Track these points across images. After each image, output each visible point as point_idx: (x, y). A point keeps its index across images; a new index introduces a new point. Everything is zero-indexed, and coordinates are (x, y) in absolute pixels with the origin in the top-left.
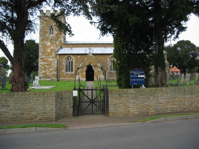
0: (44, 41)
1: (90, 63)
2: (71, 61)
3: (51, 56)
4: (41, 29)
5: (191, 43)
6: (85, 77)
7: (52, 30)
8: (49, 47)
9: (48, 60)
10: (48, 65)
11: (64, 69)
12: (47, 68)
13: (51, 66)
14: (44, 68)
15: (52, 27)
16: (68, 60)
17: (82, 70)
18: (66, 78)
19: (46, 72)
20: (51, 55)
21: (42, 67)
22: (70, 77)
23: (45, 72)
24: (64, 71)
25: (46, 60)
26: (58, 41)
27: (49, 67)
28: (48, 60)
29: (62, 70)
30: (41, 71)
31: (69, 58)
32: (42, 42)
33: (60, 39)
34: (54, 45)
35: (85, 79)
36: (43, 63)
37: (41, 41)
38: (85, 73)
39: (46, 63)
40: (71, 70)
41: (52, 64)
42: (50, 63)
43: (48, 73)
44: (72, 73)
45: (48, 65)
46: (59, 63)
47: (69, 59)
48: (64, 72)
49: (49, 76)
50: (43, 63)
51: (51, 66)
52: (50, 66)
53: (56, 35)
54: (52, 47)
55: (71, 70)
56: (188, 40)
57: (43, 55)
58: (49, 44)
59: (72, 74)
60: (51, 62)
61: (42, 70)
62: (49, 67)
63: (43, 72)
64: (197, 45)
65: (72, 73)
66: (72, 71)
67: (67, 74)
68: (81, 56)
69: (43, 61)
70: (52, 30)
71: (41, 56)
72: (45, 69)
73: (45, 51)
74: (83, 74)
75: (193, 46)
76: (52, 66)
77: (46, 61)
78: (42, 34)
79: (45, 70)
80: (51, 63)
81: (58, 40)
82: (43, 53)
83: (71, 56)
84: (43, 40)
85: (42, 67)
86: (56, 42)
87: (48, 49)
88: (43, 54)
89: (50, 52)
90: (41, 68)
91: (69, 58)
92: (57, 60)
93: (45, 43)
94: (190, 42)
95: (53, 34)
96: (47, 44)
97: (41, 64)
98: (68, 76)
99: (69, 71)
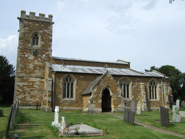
0: (25, 53)
1: (108, 86)
2: (126, 84)
3: (34, 75)
4: (21, 36)
5: (9, 64)
6: (101, 106)
7: (36, 39)
8: (31, 62)
9: (29, 80)
10: (28, 86)
11: (61, 94)
12: (27, 91)
13: (33, 89)
14: (22, 91)
15: (36, 36)
16: (67, 81)
17: (97, 97)
18: (64, 107)
19: (25, 96)
20: (34, 73)
21: (20, 90)
22: (69, 105)
23: (23, 96)
24: (61, 96)
25: (27, 79)
26: (44, 55)
27: (30, 90)
28: (29, 80)
29: (59, 96)
30: (17, 95)
31: (69, 78)
32: (21, 54)
33: (47, 53)
34: (39, 59)
35: (101, 110)
36: (21, 84)
37: (20, 52)
38: (101, 100)
39: (26, 84)
40: (126, 97)
41: (35, 86)
42: (31, 84)
43: (28, 99)
44: (72, 99)
45: (28, 86)
46: (54, 85)
47: (69, 80)
48: (62, 98)
49: (29, 103)
50: (21, 84)
51: (33, 89)
52: (32, 89)
53: (42, 47)
54: (36, 63)
55: (126, 97)
56: (173, 66)
57: (21, 73)
58: (32, 57)
59: (73, 101)
60: (33, 82)
61: (20, 94)
62: (30, 90)
63: (20, 97)
64: (182, 71)
65: (72, 99)
66: (72, 97)
67: (66, 101)
68: (84, 76)
69: (21, 81)
70: (36, 39)
71: (20, 73)
72: (24, 92)
73: (25, 67)
74: (99, 102)
75: (177, 72)
76: (35, 89)
77: (26, 81)
78: (22, 43)
79: (24, 94)
80: (33, 85)
81: (44, 54)
82: (22, 70)
83: (72, 76)
84: (22, 52)
85: (20, 90)
86: (42, 56)
87: (29, 64)
88: (22, 71)
89: (32, 68)
90: (18, 91)
91: (69, 78)
92: (52, 81)
93: (26, 55)
94: (174, 67)
95: (37, 44)
96: (30, 58)
97: (18, 86)
98: (67, 104)
99: (68, 97)
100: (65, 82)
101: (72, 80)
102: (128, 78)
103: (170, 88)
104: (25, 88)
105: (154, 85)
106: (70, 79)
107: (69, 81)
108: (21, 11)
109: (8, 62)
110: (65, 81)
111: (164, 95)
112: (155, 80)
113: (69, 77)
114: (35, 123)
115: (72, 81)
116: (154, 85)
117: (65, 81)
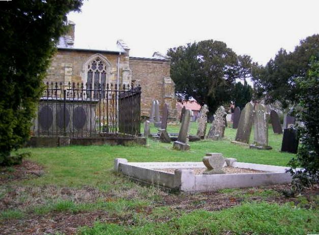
16: (94, 67)
47: (97, 66)
91: (98, 63)
100: (90, 70)
101: (104, 66)
102: (103, 56)
103: (170, 79)
104: (45, 83)
105: (101, 68)
106: (101, 65)
107: (97, 69)
108: (82, 8)
109: (250, 58)
110: (91, 68)
111: (92, 122)
112: (104, 58)
113: (98, 60)
114: (205, 130)
115: (104, 69)
116: (101, 68)
117: (91, 68)
